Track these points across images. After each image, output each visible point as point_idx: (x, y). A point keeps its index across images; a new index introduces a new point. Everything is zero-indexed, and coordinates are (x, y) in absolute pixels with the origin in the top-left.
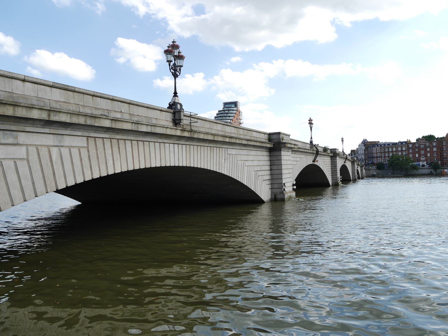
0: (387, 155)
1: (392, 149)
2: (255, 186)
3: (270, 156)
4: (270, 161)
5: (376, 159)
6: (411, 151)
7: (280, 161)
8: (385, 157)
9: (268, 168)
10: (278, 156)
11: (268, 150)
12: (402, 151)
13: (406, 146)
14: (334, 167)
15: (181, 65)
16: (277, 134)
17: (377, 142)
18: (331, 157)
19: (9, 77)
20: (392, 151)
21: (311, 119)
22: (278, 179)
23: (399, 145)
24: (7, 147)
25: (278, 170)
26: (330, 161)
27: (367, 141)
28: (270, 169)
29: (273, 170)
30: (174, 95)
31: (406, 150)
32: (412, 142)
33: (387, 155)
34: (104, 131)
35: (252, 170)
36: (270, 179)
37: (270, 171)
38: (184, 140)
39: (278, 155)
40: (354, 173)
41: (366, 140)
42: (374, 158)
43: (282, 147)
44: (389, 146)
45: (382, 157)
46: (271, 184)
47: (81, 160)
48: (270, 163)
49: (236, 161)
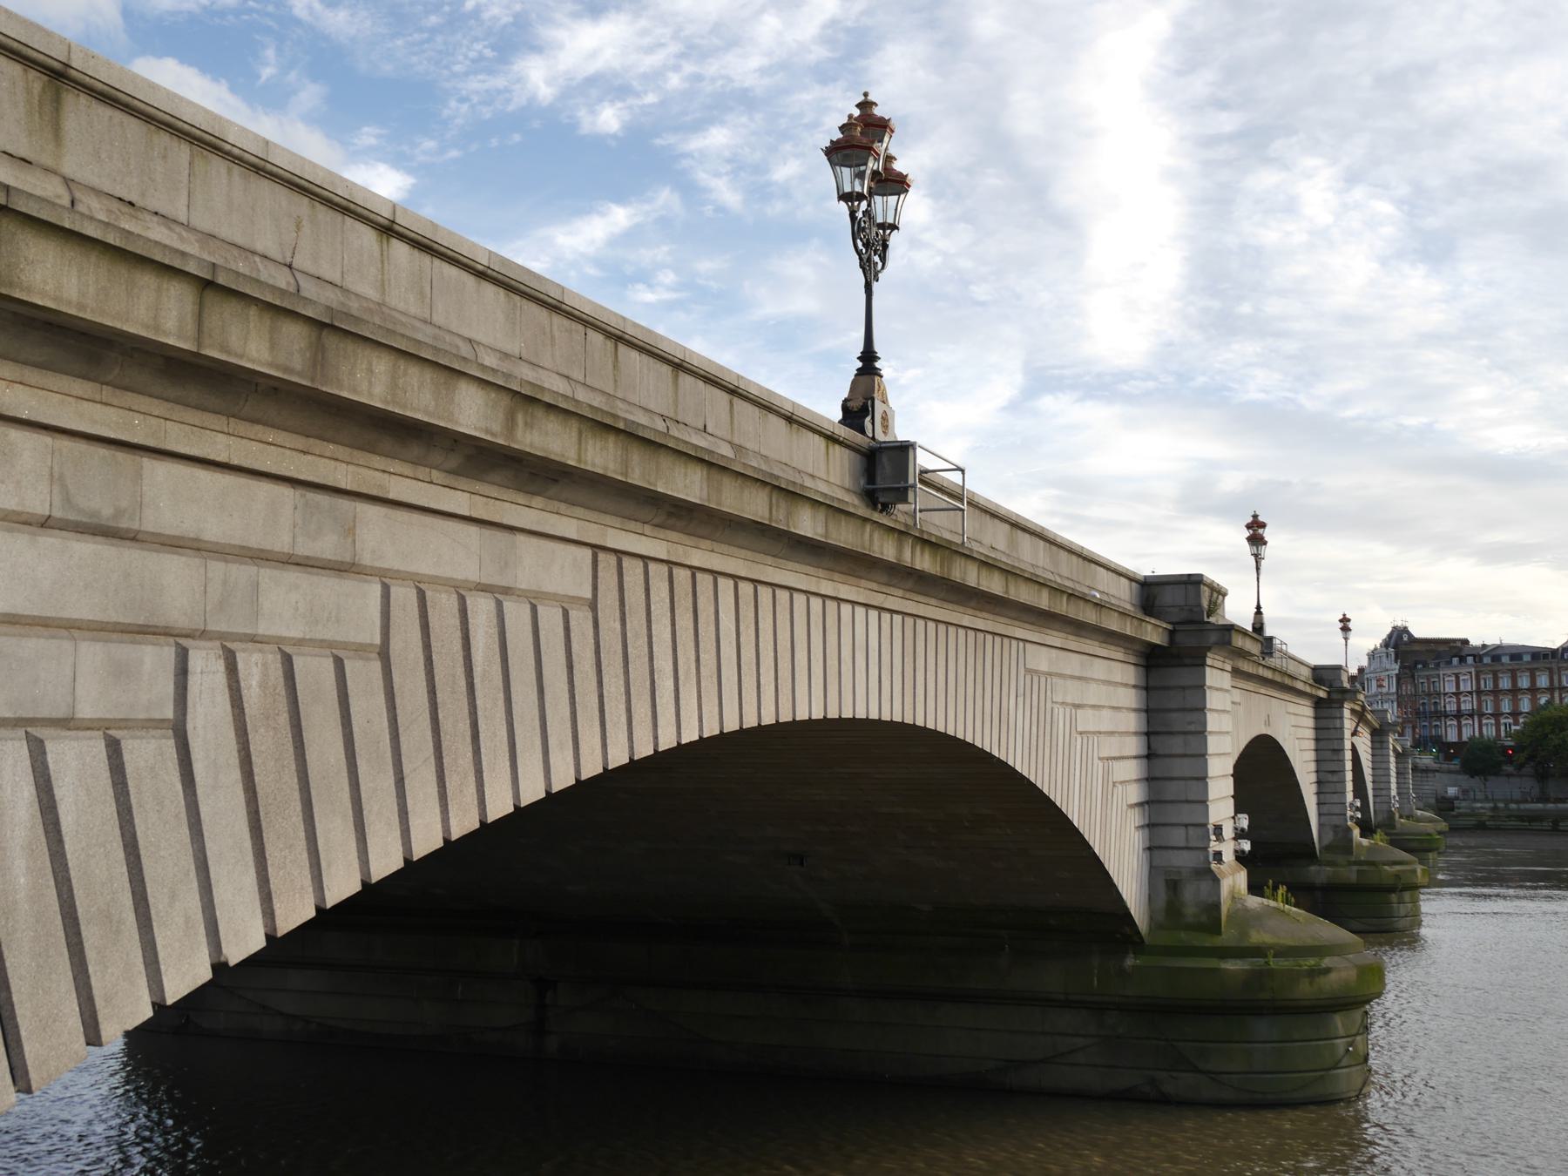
0: (1506, 707)
1: (1533, 680)
2: (1103, 833)
3: (1147, 688)
4: (1147, 711)
8: (1497, 715)
9: (1133, 746)
11: (1132, 659)
14: (1328, 755)
15: (890, 220)
16: (1185, 583)
17: (1459, 644)
18: (1318, 704)
19: (337, 205)
20: (1533, 690)
22: (1188, 802)
24: (315, 578)
25: (1186, 760)
26: (1310, 723)
28: (1146, 753)
29: (1157, 756)
30: (860, 364)
33: (1506, 707)
34: (656, 521)
35: (1096, 755)
36: (1147, 802)
37: (1145, 761)
38: (900, 593)
40: (1382, 786)
41: (1405, 630)
42: (1446, 716)
43: (1209, 649)
45: (1481, 715)
46: (1148, 826)
47: (570, 667)
48: (1144, 722)
49: (1049, 705)
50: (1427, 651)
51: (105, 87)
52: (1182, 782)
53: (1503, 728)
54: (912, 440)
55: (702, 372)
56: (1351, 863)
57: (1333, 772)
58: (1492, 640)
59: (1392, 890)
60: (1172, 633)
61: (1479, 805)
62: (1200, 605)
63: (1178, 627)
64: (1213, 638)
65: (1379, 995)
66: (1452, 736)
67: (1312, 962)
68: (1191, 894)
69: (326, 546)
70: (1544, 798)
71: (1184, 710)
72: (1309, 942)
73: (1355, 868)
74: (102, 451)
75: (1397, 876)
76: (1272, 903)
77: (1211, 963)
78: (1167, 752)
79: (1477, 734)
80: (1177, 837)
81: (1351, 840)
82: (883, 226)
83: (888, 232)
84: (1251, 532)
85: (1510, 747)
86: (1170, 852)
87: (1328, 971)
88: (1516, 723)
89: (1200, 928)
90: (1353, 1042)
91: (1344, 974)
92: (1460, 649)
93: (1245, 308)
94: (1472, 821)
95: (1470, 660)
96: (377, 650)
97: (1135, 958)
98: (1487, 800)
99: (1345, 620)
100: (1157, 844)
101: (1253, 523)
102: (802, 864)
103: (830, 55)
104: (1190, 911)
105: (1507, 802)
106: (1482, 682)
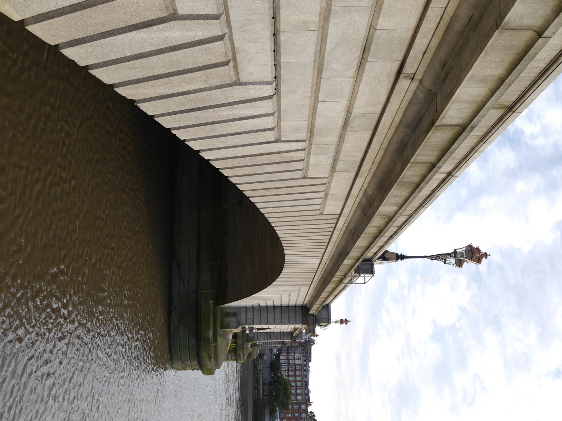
0: (291, 373)
1: (299, 381)
5: (286, 358)
6: (295, 407)
7: (287, 322)
8: (288, 370)
10: (294, 319)
12: (297, 395)
13: (303, 400)
14: (276, 335)
16: (328, 318)
17: (310, 359)
20: (296, 381)
21: (348, 323)
22: (261, 319)
23: (305, 391)
25: (273, 318)
27: (312, 345)
30: (399, 254)
31: (297, 400)
32: (308, 408)
33: (291, 373)
37: (273, 306)
39: (297, 320)
41: (314, 344)
42: (288, 356)
43: (308, 326)
44: (303, 376)
45: (288, 366)
50: (307, 350)
51: (505, 120)
52: (266, 317)
53: (284, 372)
54: (375, 275)
55: (398, 232)
56: (243, 342)
57: (270, 337)
58: (311, 369)
59: (235, 354)
60: (313, 315)
61: (261, 366)
62: (321, 323)
63: (314, 317)
64: (311, 328)
65: (203, 373)
66: (282, 357)
67: (213, 356)
68: (232, 319)
69: (340, 165)
70: (263, 384)
71: (289, 318)
72: (219, 355)
73: (241, 343)
74: (374, 123)
75: (239, 355)
76: (230, 342)
77: (212, 326)
78: (276, 313)
79: (283, 364)
80: (250, 315)
81: (250, 342)
82: (445, 260)
83: (443, 261)
84: (344, 320)
85: (279, 374)
86: (245, 313)
87: (210, 360)
88: (286, 376)
89: (222, 322)
90: (189, 366)
91: (209, 365)
92: (308, 360)
93: (418, 278)
94: (256, 364)
95: (305, 363)
96: (306, 176)
97: (212, 304)
98: (263, 368)
99: (347, 321)
100: (247, 309)
101: (347, 321)
102: (239, 204)
103: (511, 133)
104: (227, 320)
105: (262, 374)
106: (298, 366)
